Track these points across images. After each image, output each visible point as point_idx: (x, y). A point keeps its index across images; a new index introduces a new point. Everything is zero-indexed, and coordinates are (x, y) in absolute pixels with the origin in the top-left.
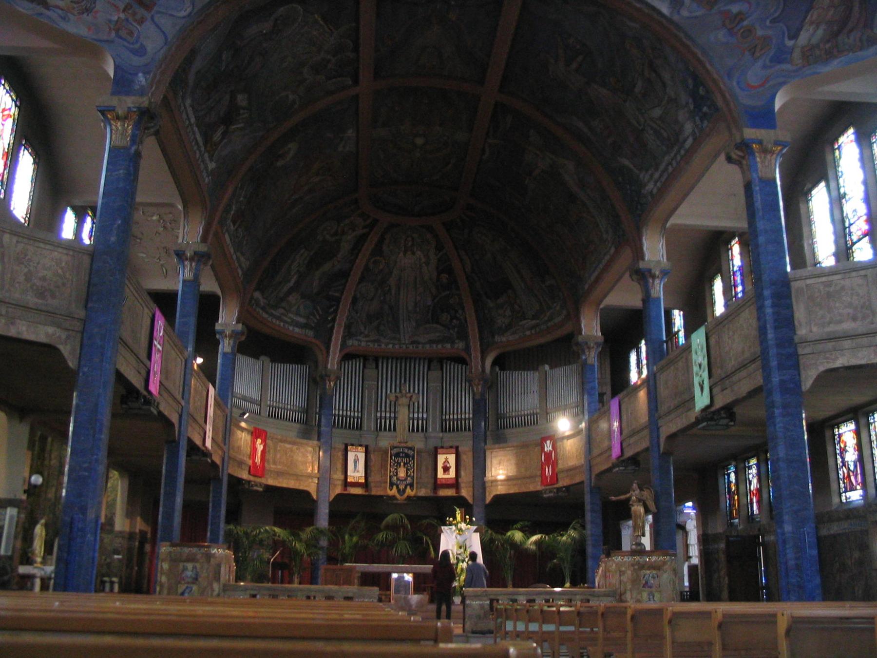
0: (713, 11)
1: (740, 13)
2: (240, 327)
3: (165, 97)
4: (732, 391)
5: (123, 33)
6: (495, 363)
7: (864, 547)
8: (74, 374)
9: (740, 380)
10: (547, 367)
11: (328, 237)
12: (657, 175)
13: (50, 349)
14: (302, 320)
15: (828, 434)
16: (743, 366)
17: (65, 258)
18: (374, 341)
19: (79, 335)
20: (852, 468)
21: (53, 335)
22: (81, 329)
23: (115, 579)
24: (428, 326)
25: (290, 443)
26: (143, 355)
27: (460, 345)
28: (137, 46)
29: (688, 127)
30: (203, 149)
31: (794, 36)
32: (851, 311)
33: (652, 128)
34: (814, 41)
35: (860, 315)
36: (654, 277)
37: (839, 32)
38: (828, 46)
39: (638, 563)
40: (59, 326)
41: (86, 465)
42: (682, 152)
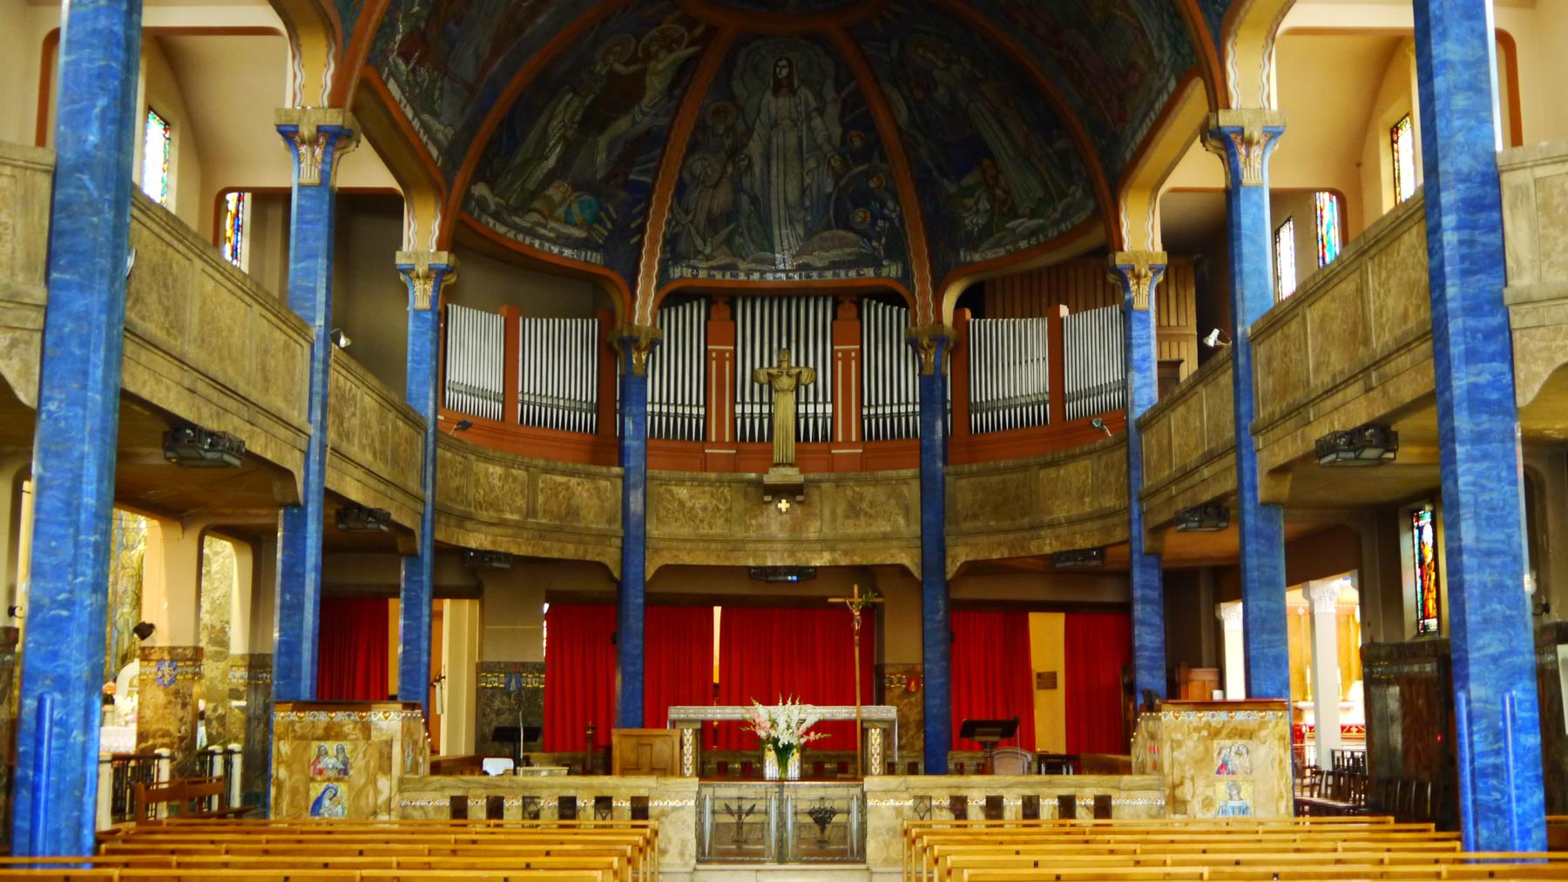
2: (444, 258)
6: (960, 304)
8: (29, 416)
9: (1398, 375)
10: (1064, 311)
11: (619, 68)
14: (579, 233)
18: (723, 268)
19: (38, 336)
22: (39, 323)
23: (234, 746)
24: (826, 234)
25: (563, 473)
27: (892, 270)
36: (1249, 143)
39: (1208, 725)
41: (62, 597)
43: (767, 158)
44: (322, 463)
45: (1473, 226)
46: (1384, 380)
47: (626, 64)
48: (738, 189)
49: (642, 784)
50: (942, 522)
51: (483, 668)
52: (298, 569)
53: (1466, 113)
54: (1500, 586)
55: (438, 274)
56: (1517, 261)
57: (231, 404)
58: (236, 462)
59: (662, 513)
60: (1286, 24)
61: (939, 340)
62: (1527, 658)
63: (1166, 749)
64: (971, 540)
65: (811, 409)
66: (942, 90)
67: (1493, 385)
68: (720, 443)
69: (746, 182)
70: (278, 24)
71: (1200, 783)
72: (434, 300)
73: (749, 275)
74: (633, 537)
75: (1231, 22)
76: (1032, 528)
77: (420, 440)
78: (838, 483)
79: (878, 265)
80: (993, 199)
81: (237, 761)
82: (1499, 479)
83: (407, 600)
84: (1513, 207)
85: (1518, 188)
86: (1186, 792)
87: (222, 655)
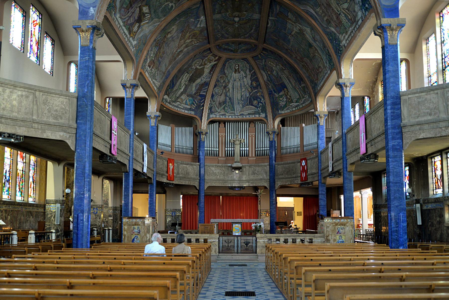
2: (158, 114)
3: (105, 16)
4: (375, 146)
7: (442, 216)
8: (73, 152)
10: (304, 125)
11: (198, 67)
13: (61, 143)
14: (189, 107)
15: (429, 161)
16: (379, 136)
17: (65, 100)
18: (222, 115)
19: (75, 135)
20: (439, 178)
21: (63, 136)
22: (75, 132)
23: (110, 228)
25: (185, 164)
26: (107, 138)
27: (263, 115)
29: (360, 14)
30: (129, 36)
32: (429, 111)
33: (344, 13)
35: (433, 113)
36: (346, 87)
42: (357, 27)
44: (133, 163)
46: (375, 143)
48: (226, 96)
49: (206, 236)
52: (128, 187)
53: (393, 82)
54: (398, 190)
55: (156, 117)
56: (404, 117)
58: (115, 163)
59: (208, 174)
60: (356, 57)
61: (274, 132)
64: (281, 180)
65: (243, 149)
66: (275, 72)
67: (397, 145)
69: (228, 94)
70: (121, 60)
71: (333, 236)
72: (155, 123)
74: (201, 179)
75: (342, 58)
77: (153, 156)
80: (287, 98)
81: (111, 231)
82: (399, 166)
83: (150, 194)
85: (405, 100)
86: (330, 238)
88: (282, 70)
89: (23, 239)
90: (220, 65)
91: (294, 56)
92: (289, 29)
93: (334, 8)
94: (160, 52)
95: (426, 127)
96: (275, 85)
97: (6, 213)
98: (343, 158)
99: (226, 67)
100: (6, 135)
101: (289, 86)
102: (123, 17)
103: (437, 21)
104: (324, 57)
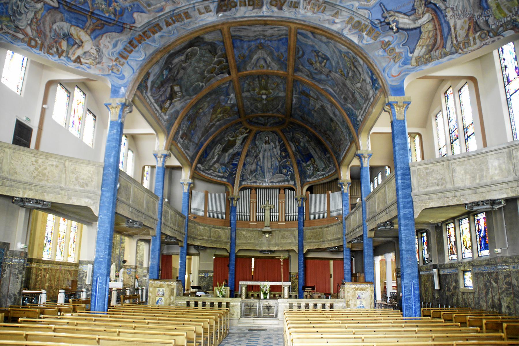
0: (377, 41)
1: (389, 41)
5: (115, 71)
6: (307, 190)
7: (457, 281)
10: (330, 192)
11: (230, 139)
12: (362, 113)
13: (87, 209)
16: (393, 204)
17: (92, 169)
18: (254, 182)
27: (292, 183)
28: (121, 75)
29: (371, 93)
30: (160, 111)
31: (412, 52)
34: (421, 55)
35: (440, 183)
36: (365, 157)
37: (431, 51)
38: (427, 56)
40: (90, 198)
42: (370, 103)
43: (264, 158)
45: (404, 179)
46: (390, 211)
47: (232, 138)
48: (257, 165)
50: (303, 240)
51: (200, 272)
54: (411, 258)
57: (140, 214)
60: (372, 131)
62: (416, 274)
63: (346, 293)
67: (409, 214)
68: (253, 222)
70: (154, 132)
71: (353, 301)
73: (259, 184)
74: (233, 243)
76: (323, 242)
78: (280, 231)
79: (289, 182)
80: (314, 167)
84: (413, 175)
86: (350, 303)
87: (142, 268)
88: (308, 142)
89: (53, 299)
90: (251, 137)
91: (318, 129)
92: (312, 105)
93: (349, 87)
94: (192, 126)
95: (434, 196)
96: (303, 155)
97: (45, 271)
98: (363, 225)
99: (257, 139)
100: (35, 201)
101: (316, 156)
102: (154, 95)
103: (443, 101)
104: (344, 131)
